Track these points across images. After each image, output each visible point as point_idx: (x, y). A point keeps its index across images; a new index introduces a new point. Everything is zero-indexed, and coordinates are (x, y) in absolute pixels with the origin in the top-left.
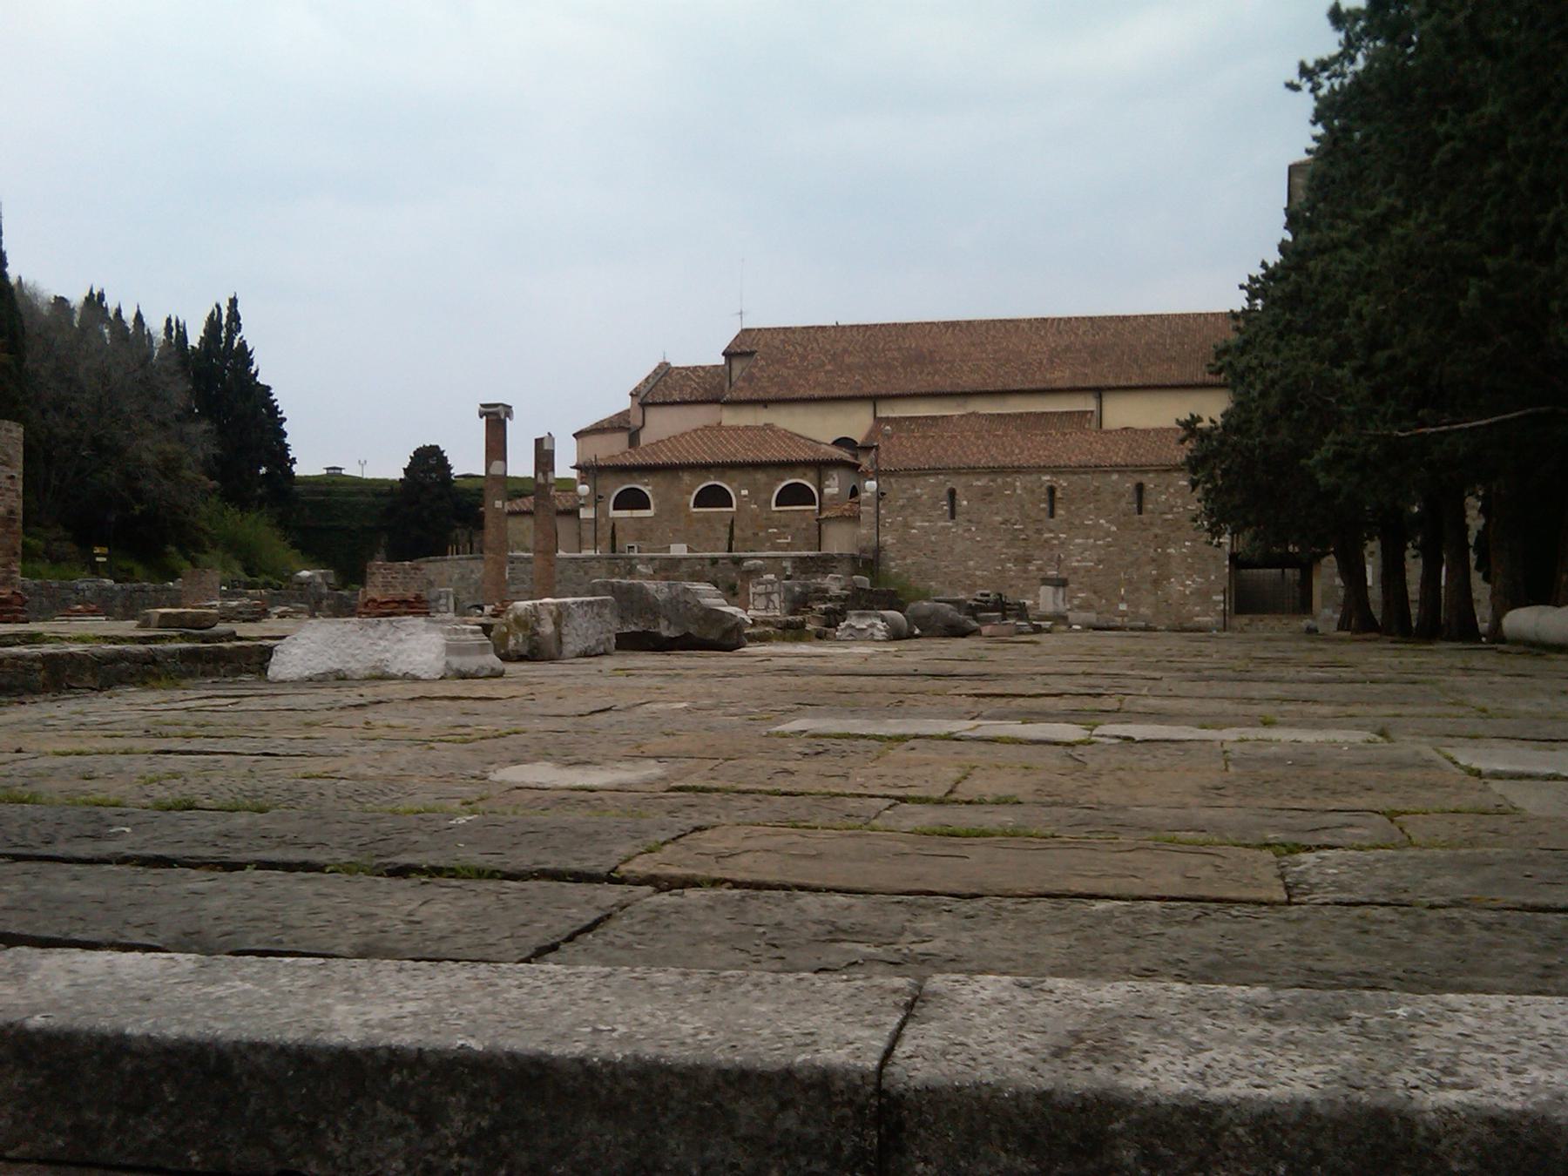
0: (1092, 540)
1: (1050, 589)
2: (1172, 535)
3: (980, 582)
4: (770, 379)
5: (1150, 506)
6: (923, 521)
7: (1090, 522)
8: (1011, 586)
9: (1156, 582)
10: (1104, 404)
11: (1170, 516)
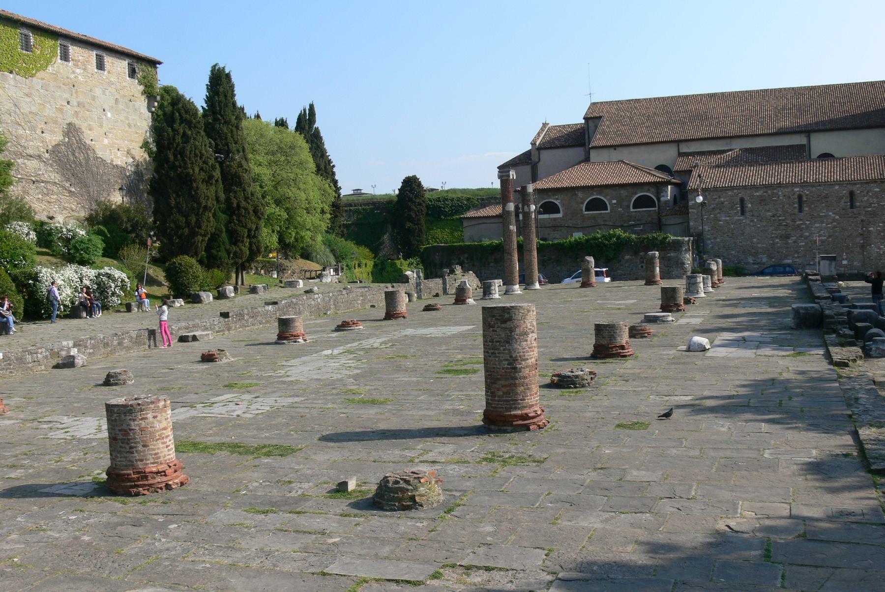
0: (825, 225)
1: (828, 262)
2: (872, 220)
3: (760, 250)
4: (615, 133)
5: (858, 204)
6: (726, 217)
7: (823, 214)
8: (779, 252)
9: (863, 247)
10: (811, 139)
11: (870, 209)
